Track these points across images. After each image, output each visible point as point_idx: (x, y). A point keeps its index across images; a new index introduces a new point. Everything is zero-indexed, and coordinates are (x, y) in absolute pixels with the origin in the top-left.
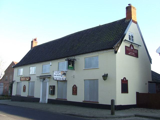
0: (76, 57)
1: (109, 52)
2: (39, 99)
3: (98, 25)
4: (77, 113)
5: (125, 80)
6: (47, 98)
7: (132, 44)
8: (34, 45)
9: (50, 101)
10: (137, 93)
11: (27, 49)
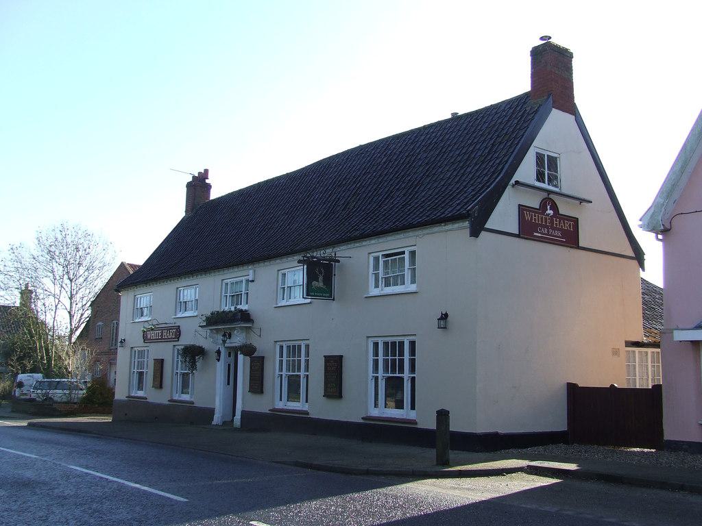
0: (344, 253)
2: (211, 412)
3: (438, 112)
4: (564, 468)
7: (551, 196)
9: (253, 421)
11: (171, 212)
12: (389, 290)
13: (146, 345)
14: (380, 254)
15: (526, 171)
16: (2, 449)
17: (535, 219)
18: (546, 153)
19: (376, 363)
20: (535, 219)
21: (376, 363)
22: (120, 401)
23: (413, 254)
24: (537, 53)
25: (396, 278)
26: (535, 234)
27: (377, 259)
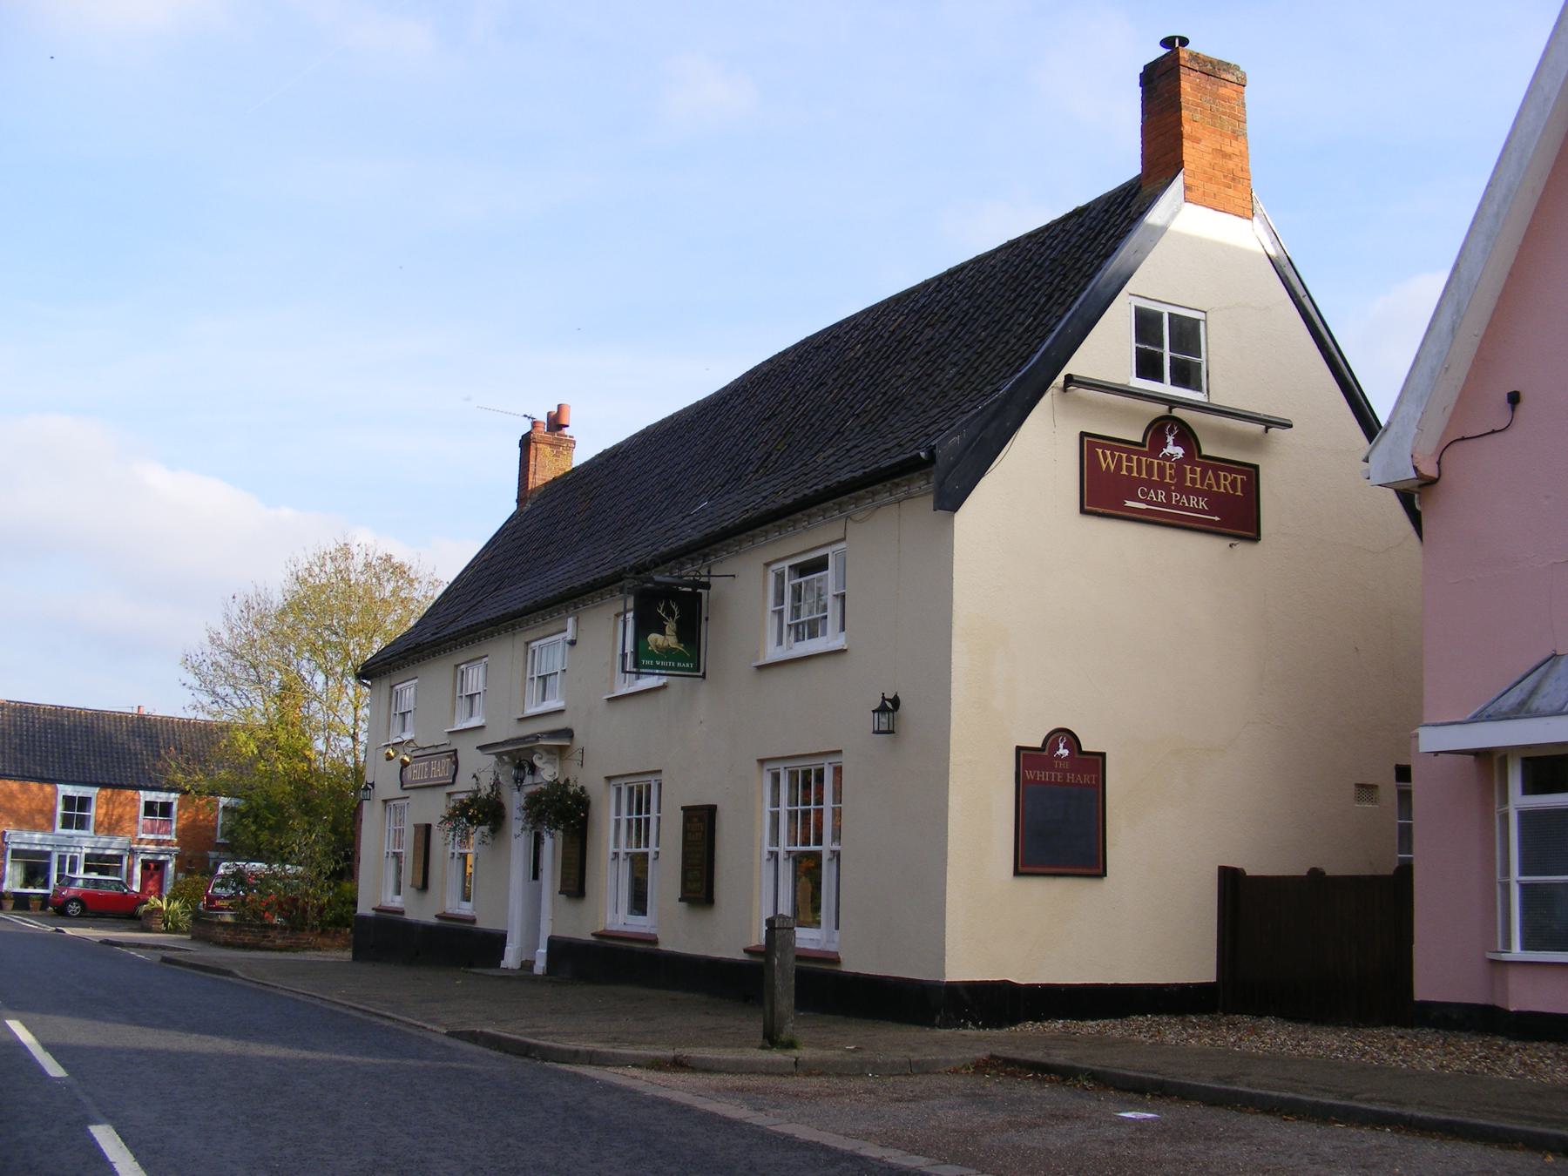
1: (910, 497)
2: (497, 942)
5: (1063, 752)
6: (546, 931)
8: (547, 469)
10: (1230, 880)
13: (407, 793)
14: (786, 565)
15: (1107, 350)
17: (1129, 469)
18: (1166, 310)
20: (1129, 469)
22: (364, 918)
26: (1129, 504)
27: (780, 577)
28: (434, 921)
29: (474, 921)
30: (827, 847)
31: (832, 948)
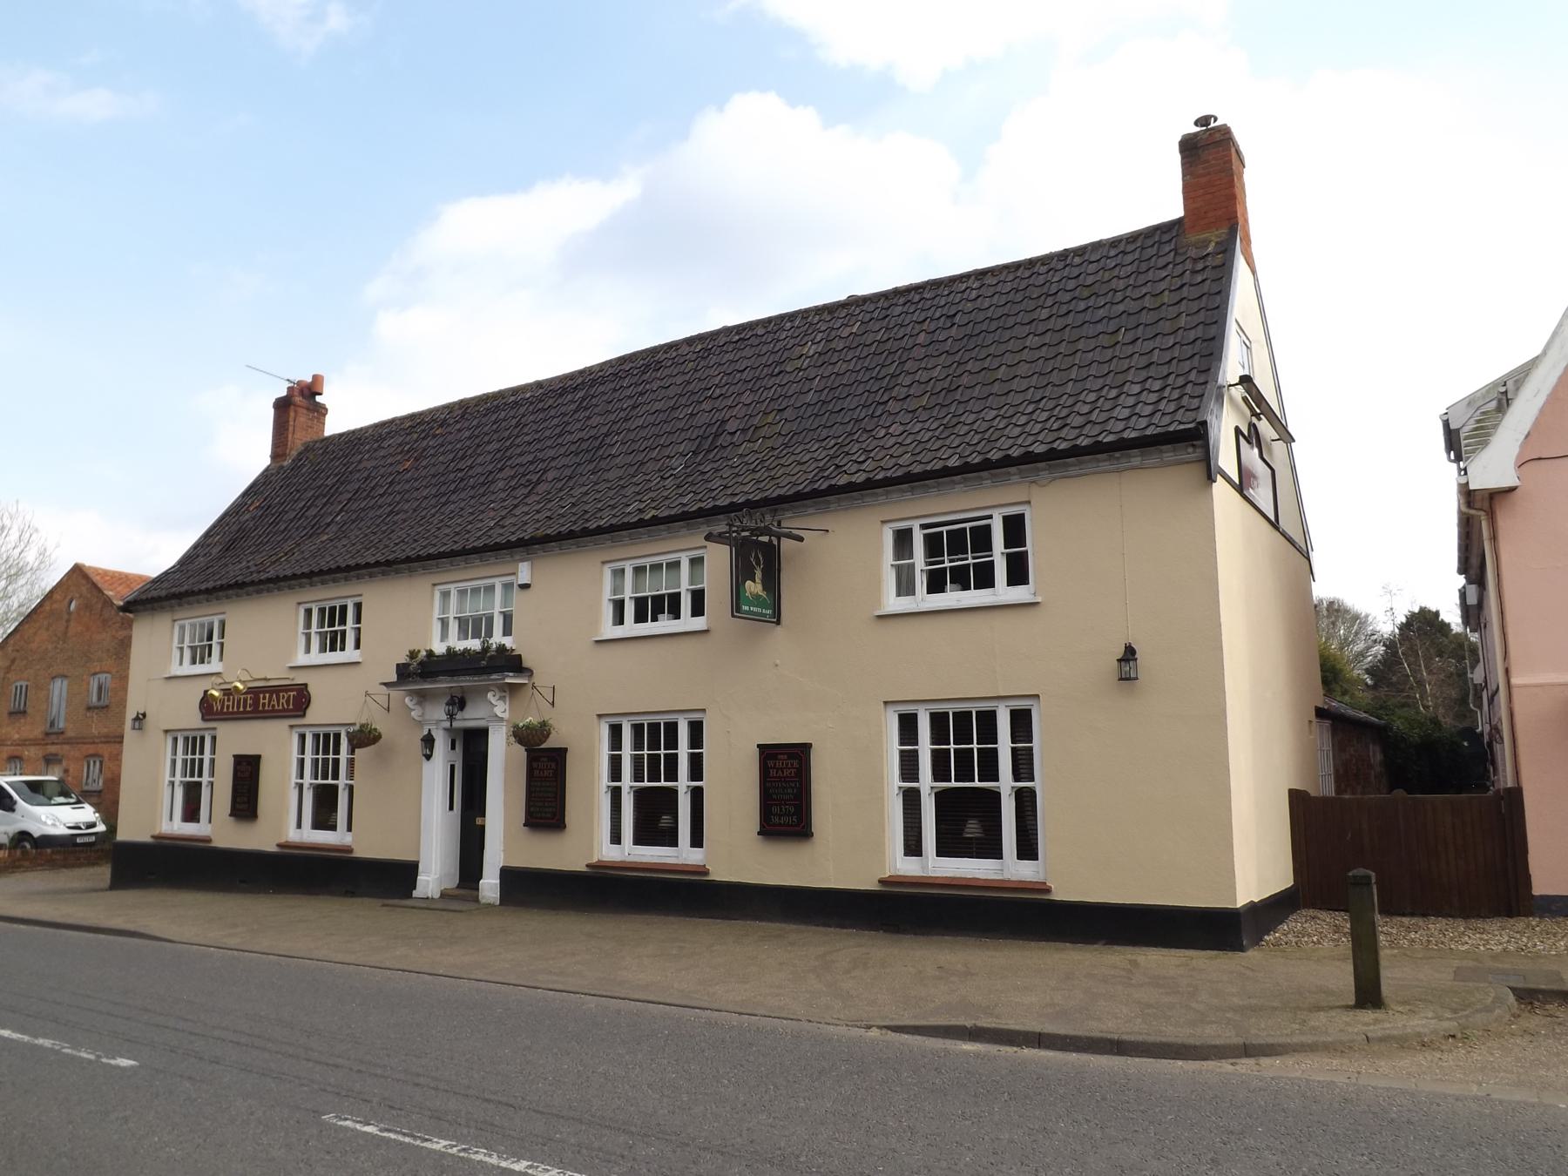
11: (249, 454)
12: (648, 628)
16: (6, 1033)
19: (616, 763)
21: (616, 763)
23: (358, 606)
24: (1189, 147)
25: (658, 600)
28: (584, 869)
29: (209, 840)
30: (205, 779)
31: (1039, 878)
